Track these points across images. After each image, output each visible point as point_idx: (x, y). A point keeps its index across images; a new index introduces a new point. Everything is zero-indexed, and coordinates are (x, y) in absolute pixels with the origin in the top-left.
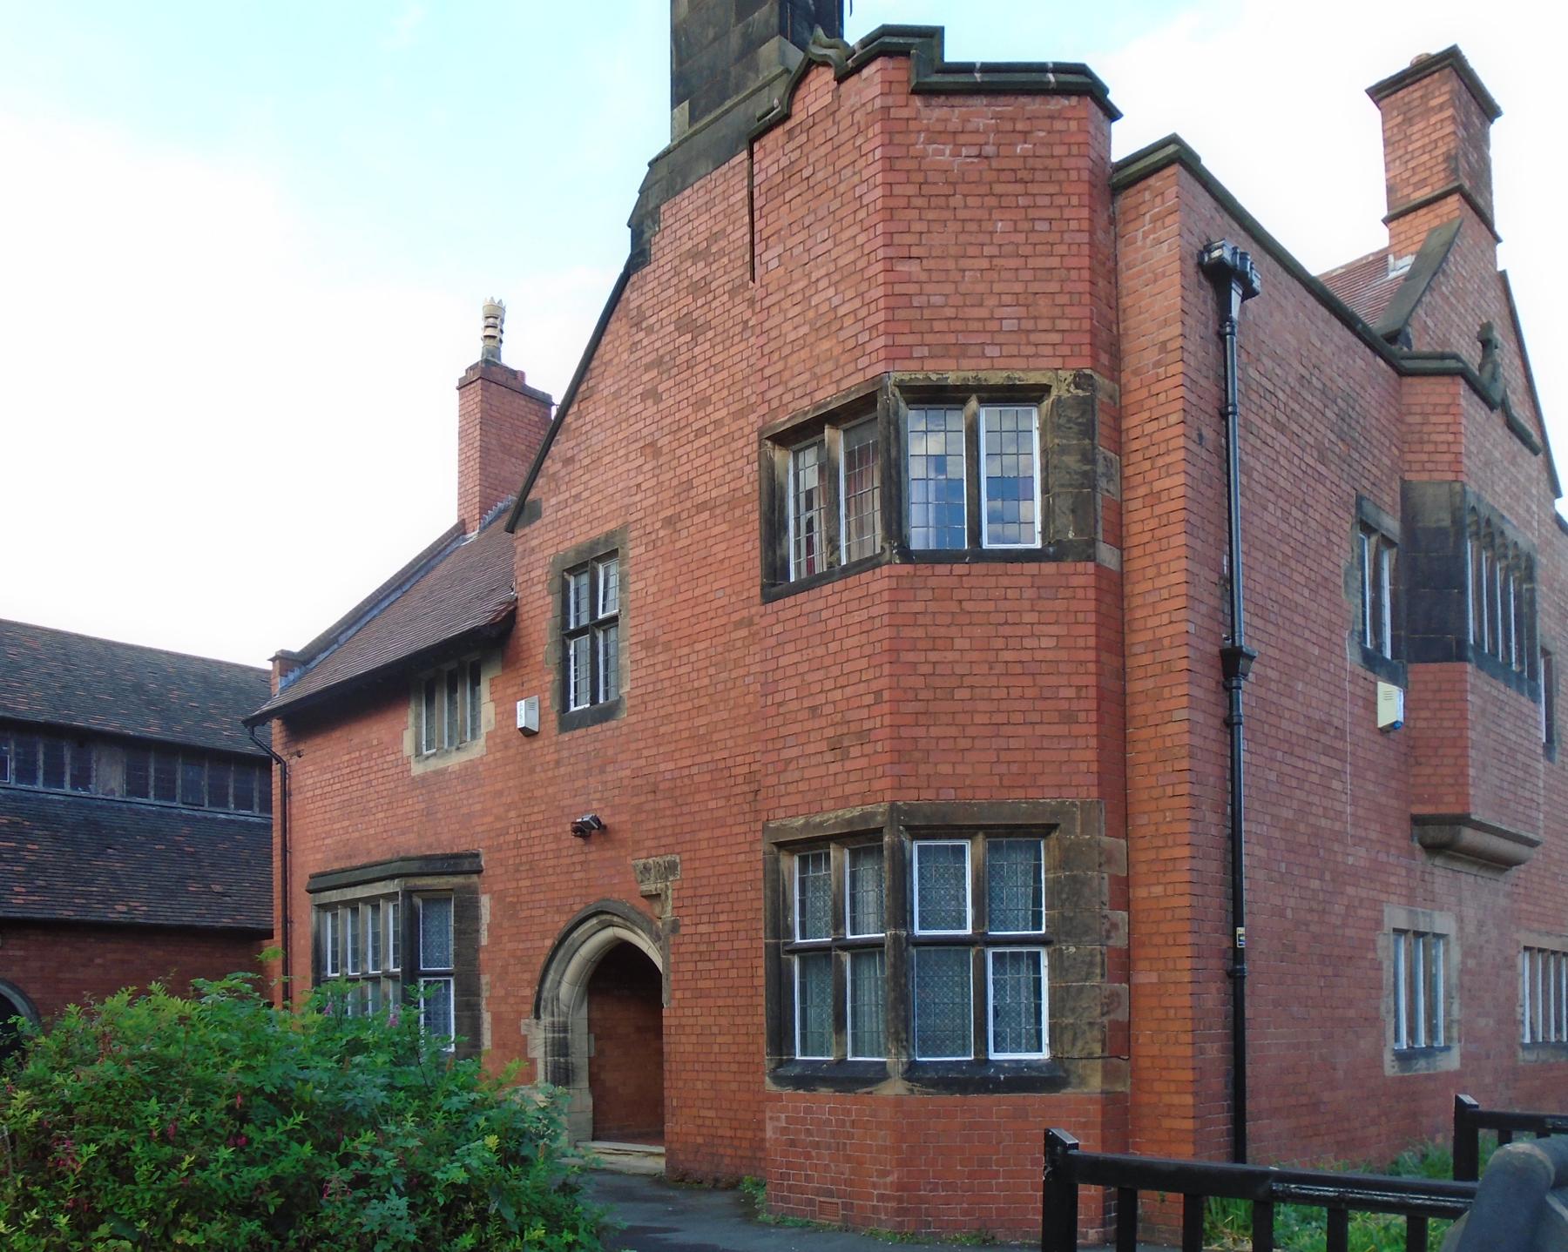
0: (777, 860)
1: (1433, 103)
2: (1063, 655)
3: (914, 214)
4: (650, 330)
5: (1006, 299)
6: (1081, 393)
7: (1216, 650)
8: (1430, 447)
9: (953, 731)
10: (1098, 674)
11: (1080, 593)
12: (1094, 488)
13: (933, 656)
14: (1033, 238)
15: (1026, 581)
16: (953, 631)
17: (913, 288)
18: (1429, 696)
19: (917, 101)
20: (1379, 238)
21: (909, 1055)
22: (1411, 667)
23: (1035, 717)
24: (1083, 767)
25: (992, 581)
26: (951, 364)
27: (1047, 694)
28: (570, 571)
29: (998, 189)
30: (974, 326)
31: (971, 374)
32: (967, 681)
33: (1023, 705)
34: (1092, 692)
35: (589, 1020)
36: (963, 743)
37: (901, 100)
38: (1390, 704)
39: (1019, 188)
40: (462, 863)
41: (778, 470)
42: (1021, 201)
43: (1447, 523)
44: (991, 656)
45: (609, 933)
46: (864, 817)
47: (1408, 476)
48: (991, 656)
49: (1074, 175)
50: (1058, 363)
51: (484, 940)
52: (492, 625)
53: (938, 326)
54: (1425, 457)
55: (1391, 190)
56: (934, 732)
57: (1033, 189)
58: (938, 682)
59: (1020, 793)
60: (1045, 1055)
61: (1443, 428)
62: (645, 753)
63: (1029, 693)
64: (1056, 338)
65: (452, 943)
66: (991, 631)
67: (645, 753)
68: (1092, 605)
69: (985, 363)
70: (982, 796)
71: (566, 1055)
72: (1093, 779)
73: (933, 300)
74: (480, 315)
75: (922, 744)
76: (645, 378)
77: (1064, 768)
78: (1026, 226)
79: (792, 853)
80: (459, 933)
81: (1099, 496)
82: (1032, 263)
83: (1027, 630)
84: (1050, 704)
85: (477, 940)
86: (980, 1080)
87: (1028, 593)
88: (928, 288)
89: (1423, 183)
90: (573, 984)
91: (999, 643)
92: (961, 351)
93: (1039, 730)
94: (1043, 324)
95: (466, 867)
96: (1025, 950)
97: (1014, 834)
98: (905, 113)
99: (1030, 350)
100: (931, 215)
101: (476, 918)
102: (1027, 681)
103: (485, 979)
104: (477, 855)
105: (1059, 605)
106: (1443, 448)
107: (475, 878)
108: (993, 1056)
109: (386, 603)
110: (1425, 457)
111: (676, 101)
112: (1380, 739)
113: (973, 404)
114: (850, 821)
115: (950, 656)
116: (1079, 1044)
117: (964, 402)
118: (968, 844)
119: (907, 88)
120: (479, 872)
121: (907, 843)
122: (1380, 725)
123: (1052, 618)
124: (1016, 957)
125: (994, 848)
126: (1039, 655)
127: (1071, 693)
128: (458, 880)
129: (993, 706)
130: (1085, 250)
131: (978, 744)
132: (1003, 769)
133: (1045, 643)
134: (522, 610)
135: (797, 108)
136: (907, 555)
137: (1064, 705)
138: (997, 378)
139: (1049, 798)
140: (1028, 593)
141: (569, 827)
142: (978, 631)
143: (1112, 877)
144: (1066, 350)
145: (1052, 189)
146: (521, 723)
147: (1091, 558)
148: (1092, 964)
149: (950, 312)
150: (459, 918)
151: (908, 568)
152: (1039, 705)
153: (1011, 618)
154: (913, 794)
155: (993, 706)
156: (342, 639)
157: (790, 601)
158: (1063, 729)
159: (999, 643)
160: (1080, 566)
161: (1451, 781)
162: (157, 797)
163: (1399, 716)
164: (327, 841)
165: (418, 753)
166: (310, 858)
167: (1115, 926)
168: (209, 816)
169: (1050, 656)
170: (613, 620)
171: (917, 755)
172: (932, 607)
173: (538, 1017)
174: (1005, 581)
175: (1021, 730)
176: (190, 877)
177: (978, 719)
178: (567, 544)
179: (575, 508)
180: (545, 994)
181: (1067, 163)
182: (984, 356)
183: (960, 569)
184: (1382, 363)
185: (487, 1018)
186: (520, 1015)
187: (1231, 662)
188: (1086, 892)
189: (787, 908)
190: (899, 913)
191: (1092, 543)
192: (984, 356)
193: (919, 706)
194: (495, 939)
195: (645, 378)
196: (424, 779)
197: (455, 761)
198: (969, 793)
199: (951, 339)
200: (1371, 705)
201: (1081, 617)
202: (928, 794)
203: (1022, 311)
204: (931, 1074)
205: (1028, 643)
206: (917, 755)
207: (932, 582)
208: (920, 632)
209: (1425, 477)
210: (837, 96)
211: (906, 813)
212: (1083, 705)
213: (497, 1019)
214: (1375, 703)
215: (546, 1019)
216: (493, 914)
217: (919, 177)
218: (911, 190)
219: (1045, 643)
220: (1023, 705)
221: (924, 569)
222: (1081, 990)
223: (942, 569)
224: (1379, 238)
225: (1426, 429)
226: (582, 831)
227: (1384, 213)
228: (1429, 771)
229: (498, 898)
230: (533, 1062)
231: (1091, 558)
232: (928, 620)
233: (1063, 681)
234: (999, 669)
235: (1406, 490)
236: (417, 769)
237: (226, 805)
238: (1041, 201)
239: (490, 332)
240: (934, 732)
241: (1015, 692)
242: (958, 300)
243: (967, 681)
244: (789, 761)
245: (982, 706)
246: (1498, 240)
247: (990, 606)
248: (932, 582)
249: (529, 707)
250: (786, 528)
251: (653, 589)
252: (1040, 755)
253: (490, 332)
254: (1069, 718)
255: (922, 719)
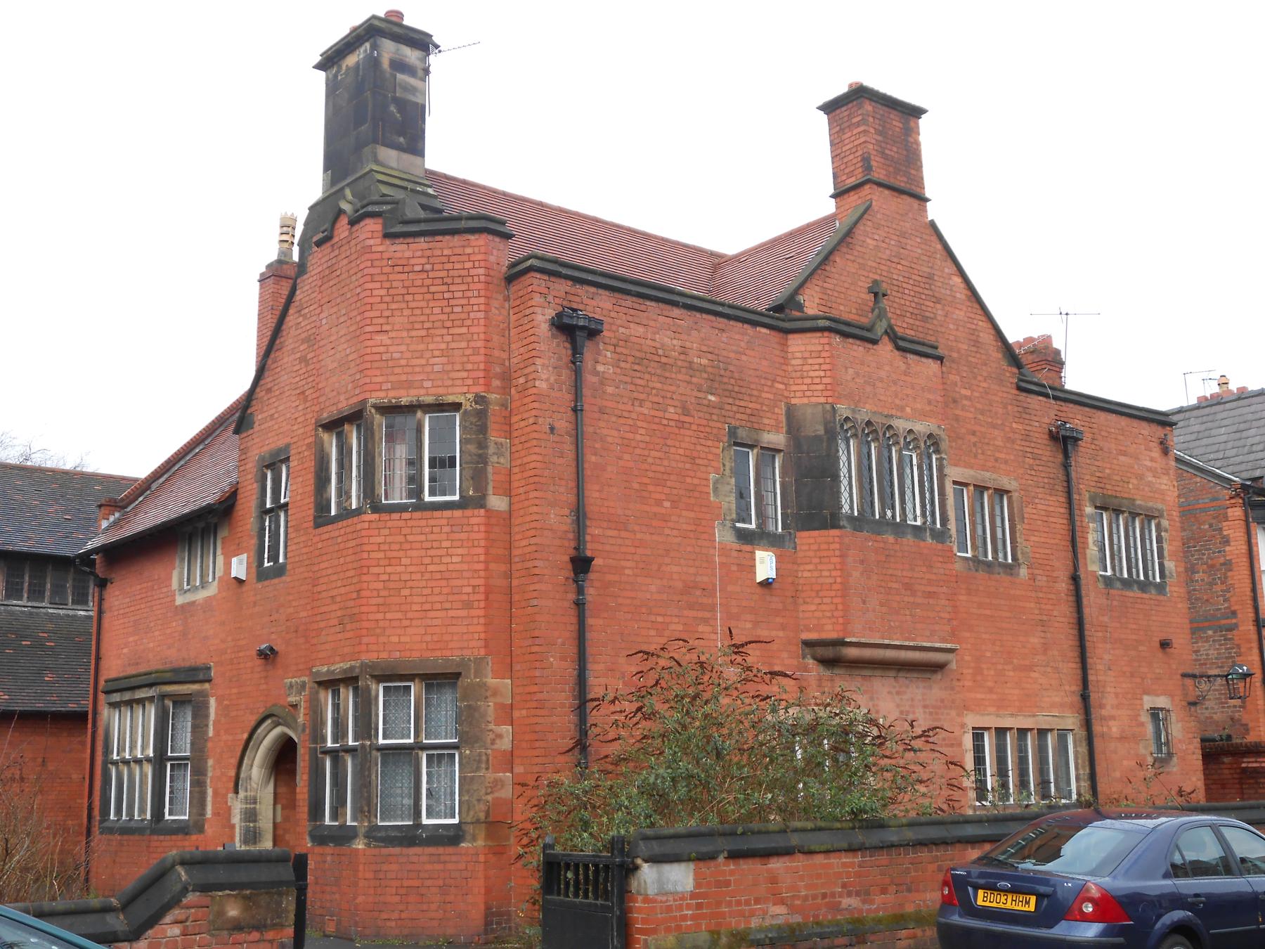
0: (317, 693)
1: (855, 120)
2: (465, 567)
3: (385, 306)
4: (304, 316)
5: (437, 353)
6: (478, 407)
7: (567, 558)
8: (808, 381)
9: (399, 615)
10: (487, 578)
11: (476, 528)
12: (486, 463)
13: (389, 569)
14: (452, 317)
15: (444, 522)
16: (401, 554)
17: (382, 349)
18: (811, 554)
19: (388, 242)
20: (829, 207)
21: (370, 821)
22: (798, 534)
23: (448, 605)
24: (476, 636)
25: (423, 523)
26: (402, 392)
27: (455, 591)
28: (267, 467)
29: (433, 289)
30: (417, 369)
31: (414, 399)
32: (409, 584)
33: (441, 598)
34: (482, 589)
35: (275, 794)
36: (407, 623)
37: (379, 241)
38: (765, 565)
39: (445, 288)
40: (197, 674)
41: (326, 445)
42: (446, 295)
43: (821, 432)
44: (422, 568)
45: (278, 730)
46: (352, 668)
47: (794, 401)
48: (422, 568)
49: (476, 279)
50: (465, 389)
51: (211, 734)
52: (220, 502)
53: (397, 370)
54: (805, 388)
55: (835, 176)
56: (389, 616)
57: (452, 288)
58: (392, 585)
59: (438, 653)
60: (456, 821)
61: (817, 367)
62: (294, 604)
63: (445, 591)
64: (465, 374)
65: (189, 735)
66: (423, 553)
67: (294, 604)
68: (482, 535)
69: (422, 392)
70: (415, 655)
71: (255, 821)
72: (482, 643)
73: (395, 355)
74: (278, 224)
75: (381, 624)
76: (302, 348)
77: (465, 637)
78: (448, 310)
79: (327, 689)
80: (194, 727)
81: (490, 469)
82: (451, 331)
83: (443, 552)
84: (456, 597)
85: (206, 732)
86: (411, 837)
87: (446, 529)
88: (391, 349)
89: (850, 175)
90: (261, 767)
91: (427, 560)
92: (409, 385)
93: (451, 613)
94: (458, 367)
95: (201, 677)
96: (446, 752)
97: (440, 679)
98: (380, 248)
99: (450, 383)
100: (394, 306)
101: (207, 716)
102: (444, 583)
103: (210, 762)
104: (209, 669)
105: (463, 536)
106: (817, 381)
107: (207, 686)
108: (425, 821)
109: (182, 462)
110: (805, 388)
111: (326, 169)
112: (759, 590)
113: (419, 414)
114: (345, 671)
115: (399, 569)
116: (472, 813)
117: (415, 412)
118: (412, 684)
119: (380, 235)
120: (209, 681)
121: (374, 687)
122: (759, 579)
123: (459, 544)
124: (440, 756)
125: (429, 688)
126: (451, 567)
127: (469, 590)
128: (196, 687)
129: (424, 599)
130: (482, 322)
131: (414, 623)
132: (428, 638)
133: (455, 559)
134: (240, 491)
135: (336, 233)
136: (377, 508)
137: (465, 597)
138: (429, 399)
139: (455, 656)
140: (446, 529)
141: (254, 653)
142: (414, 553)
143: (495, 704)
144: (470, 382)
145: (464, 287)
146: (233, 575)
147: (483, 506)
148: (480, 761)
149: (403, 362)
150: (195, 717)
151: (376, 516)
152: (451, 598)
153: (435, 545)
154: (375, 655)
155: (424, 599)
156: (154, 486)
157: (330, 527)
158: (463, 613)
159: (427, 560)
160: (476, 512)
161: (829, 614)
162: (29, 599)
163: (772, 574)
164: (125, 651)
165: (181, 588)
166: (113, 667)
167: (500, 736)
168: (71, 613)
169: (458, 567)
170: (286, 504)
171: (378, 631)
172: (389, 539)
173: (237, 792)
174: (432, 522)
175: (439, 614)
176: (47, 668)
177: (415, 607)
178: (265, 448)
179: (270, 424)
180: (242, 775)
181: (473, 272)
182: (422, 387)
183: (406, 515)
184: (764, 330)
185: (210, 791)
186: (227, 793)
187: (581, 565)
188: (477, 715)
189: (323, 723)
190: (366, 727)
191: (484, 497)
192: (422, 387)
193: (380, 601)
194: (217, 733)
195: (302, 348)
196: (182, 606)
197: (201, 595)
198: (408, 654)
199: (404, 378)
200: (752, 568)
201: (476, 543)
202: (384, 655)
203: (444, 360)
204: (383, 834)
205: (445, 560)
206: (378, 631)
207: (389, 524)
208: (381, 555)
209: (805, 401)
210: (351, 233)
211: (370, 667)
212: (477, 597)
213: (215, 793)
214: (754, 566)
215: (242, 794)
216: (217, 714)
217: (387, 285)
218: (383, 292)
219: (455, 559)
220: (441, 598)
221: (385, 516)
222: (472, 778)
223: (395, 516)
224: (829, 207)
225: (805, 368)
226: (262, 654)
227: (832, 191)
228: (813, 608)
229: (219, 702)
230: (233, 827)
231: (483, 506)
232: (386, 547)
233: (465, 582)
234: (427, 576)
235: (791, 412)
236: (179, 600)
237: (86, 603)
238: (457, 295)
239: (285, 237)
240: (389, 616)
241: (437, 590)
242: (409, 355)
243: (409, 584)
244: (322, 629)
245: (416, 599)
246: (927, 200)
247: (423, 538)
248: (389, 524)
249: (240, 562)
250: (329, 480)
251: (300, 491)
252: (451, 629)
253: (285, 237)
254: (468, 605)
255: (382, 609)
